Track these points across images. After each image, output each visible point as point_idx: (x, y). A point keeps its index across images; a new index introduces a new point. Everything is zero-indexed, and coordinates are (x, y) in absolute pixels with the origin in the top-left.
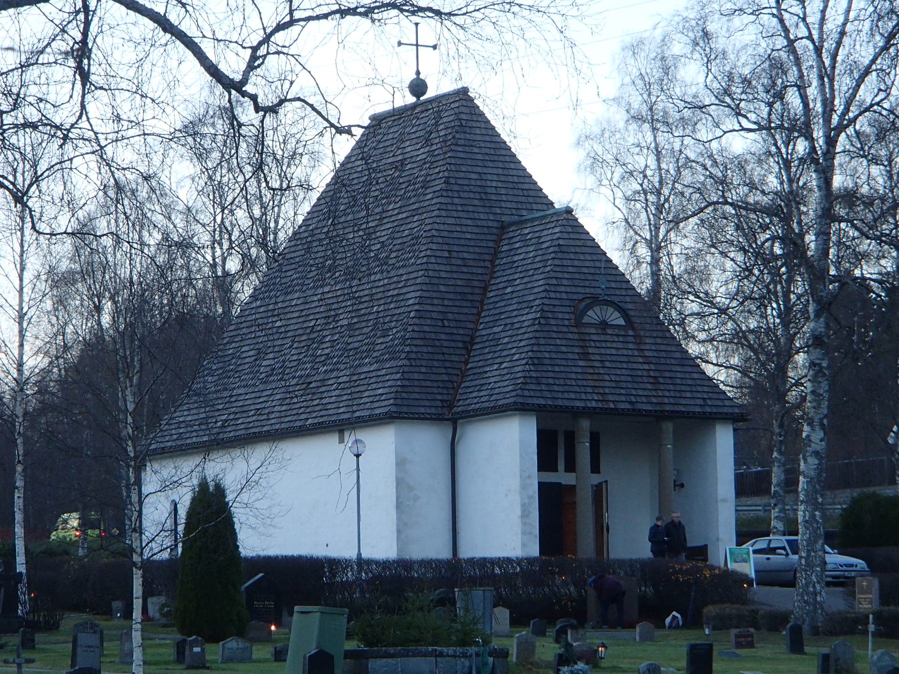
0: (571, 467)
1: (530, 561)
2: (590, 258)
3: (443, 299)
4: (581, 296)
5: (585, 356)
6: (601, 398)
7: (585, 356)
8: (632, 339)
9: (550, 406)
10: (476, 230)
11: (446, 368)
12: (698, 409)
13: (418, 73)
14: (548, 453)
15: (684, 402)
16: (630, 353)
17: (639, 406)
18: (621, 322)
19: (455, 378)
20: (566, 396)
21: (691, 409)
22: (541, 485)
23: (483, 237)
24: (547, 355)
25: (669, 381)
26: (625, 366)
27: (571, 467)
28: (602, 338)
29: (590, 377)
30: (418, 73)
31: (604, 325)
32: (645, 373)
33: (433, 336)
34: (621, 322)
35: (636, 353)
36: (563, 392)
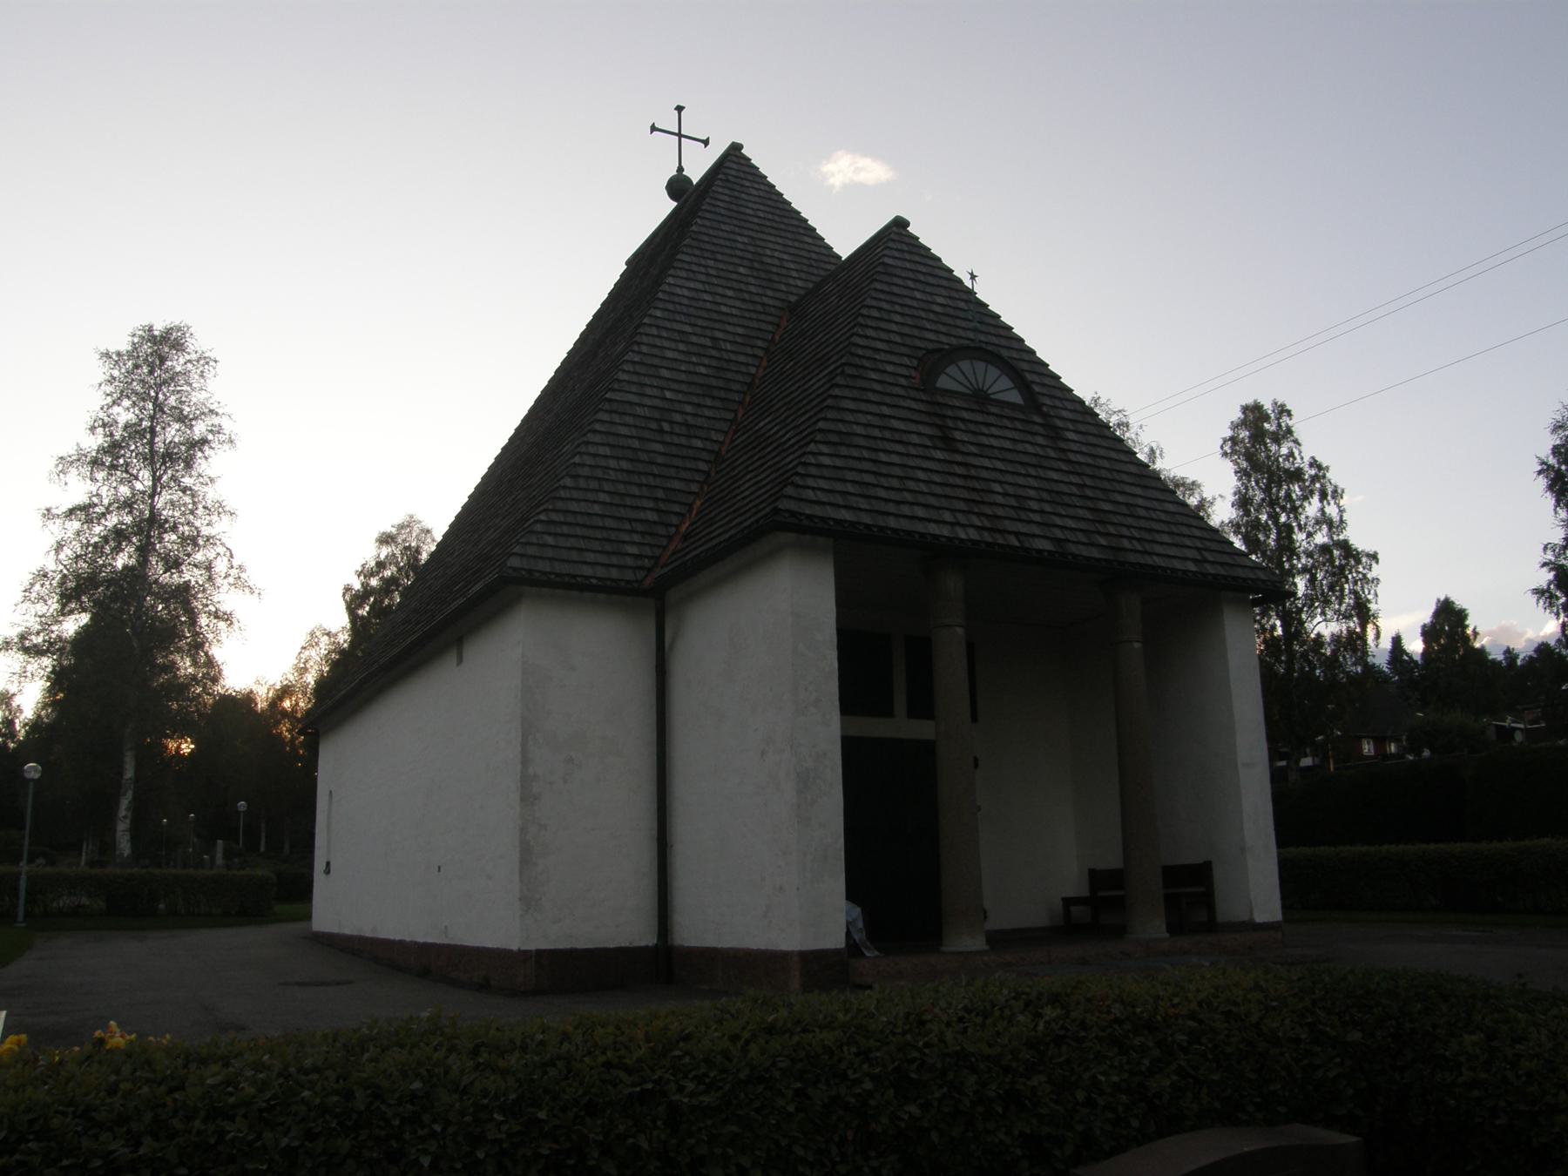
0: (922, 706)
1: (837, 952)
2: (916, 508)
3: (662, 389)
4: (931, 346)
5: (948, 443)
6: (988, 525)
7: (948, 443)
8: (1041, 430)
9: (867, 526)
10: (738, 303)
11: (656, 499)
12: (1192, 567)
13: (680, 169)
14: (870, 666)
15: (1159, 549)
16: (1039, 451)
17: (1073, 548)
18: (1015, 397)
19: (675, 520)
20: (906, 510)
21: (1178, 565)
22: (852, 748)
23: (754, 316)
24: (859, 430)
25: (1124, 510)
26: (1032, 471)
27: (922, 706)
28: (979, 418)
29: (959, 481)
30: (680, 169)
31: (980, 398)
32: (1074, 490)
33: (636, 444)
34: (1015, 397)
35: (1052, 454)
36: (898, 503)
